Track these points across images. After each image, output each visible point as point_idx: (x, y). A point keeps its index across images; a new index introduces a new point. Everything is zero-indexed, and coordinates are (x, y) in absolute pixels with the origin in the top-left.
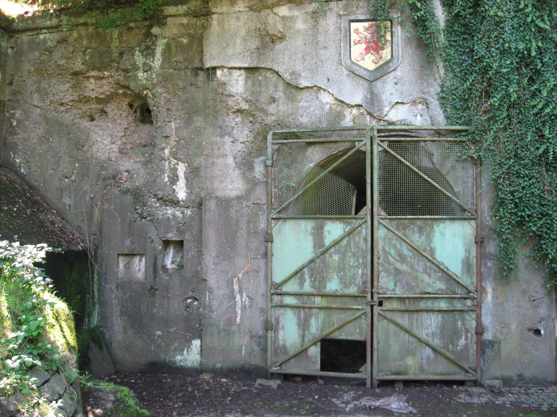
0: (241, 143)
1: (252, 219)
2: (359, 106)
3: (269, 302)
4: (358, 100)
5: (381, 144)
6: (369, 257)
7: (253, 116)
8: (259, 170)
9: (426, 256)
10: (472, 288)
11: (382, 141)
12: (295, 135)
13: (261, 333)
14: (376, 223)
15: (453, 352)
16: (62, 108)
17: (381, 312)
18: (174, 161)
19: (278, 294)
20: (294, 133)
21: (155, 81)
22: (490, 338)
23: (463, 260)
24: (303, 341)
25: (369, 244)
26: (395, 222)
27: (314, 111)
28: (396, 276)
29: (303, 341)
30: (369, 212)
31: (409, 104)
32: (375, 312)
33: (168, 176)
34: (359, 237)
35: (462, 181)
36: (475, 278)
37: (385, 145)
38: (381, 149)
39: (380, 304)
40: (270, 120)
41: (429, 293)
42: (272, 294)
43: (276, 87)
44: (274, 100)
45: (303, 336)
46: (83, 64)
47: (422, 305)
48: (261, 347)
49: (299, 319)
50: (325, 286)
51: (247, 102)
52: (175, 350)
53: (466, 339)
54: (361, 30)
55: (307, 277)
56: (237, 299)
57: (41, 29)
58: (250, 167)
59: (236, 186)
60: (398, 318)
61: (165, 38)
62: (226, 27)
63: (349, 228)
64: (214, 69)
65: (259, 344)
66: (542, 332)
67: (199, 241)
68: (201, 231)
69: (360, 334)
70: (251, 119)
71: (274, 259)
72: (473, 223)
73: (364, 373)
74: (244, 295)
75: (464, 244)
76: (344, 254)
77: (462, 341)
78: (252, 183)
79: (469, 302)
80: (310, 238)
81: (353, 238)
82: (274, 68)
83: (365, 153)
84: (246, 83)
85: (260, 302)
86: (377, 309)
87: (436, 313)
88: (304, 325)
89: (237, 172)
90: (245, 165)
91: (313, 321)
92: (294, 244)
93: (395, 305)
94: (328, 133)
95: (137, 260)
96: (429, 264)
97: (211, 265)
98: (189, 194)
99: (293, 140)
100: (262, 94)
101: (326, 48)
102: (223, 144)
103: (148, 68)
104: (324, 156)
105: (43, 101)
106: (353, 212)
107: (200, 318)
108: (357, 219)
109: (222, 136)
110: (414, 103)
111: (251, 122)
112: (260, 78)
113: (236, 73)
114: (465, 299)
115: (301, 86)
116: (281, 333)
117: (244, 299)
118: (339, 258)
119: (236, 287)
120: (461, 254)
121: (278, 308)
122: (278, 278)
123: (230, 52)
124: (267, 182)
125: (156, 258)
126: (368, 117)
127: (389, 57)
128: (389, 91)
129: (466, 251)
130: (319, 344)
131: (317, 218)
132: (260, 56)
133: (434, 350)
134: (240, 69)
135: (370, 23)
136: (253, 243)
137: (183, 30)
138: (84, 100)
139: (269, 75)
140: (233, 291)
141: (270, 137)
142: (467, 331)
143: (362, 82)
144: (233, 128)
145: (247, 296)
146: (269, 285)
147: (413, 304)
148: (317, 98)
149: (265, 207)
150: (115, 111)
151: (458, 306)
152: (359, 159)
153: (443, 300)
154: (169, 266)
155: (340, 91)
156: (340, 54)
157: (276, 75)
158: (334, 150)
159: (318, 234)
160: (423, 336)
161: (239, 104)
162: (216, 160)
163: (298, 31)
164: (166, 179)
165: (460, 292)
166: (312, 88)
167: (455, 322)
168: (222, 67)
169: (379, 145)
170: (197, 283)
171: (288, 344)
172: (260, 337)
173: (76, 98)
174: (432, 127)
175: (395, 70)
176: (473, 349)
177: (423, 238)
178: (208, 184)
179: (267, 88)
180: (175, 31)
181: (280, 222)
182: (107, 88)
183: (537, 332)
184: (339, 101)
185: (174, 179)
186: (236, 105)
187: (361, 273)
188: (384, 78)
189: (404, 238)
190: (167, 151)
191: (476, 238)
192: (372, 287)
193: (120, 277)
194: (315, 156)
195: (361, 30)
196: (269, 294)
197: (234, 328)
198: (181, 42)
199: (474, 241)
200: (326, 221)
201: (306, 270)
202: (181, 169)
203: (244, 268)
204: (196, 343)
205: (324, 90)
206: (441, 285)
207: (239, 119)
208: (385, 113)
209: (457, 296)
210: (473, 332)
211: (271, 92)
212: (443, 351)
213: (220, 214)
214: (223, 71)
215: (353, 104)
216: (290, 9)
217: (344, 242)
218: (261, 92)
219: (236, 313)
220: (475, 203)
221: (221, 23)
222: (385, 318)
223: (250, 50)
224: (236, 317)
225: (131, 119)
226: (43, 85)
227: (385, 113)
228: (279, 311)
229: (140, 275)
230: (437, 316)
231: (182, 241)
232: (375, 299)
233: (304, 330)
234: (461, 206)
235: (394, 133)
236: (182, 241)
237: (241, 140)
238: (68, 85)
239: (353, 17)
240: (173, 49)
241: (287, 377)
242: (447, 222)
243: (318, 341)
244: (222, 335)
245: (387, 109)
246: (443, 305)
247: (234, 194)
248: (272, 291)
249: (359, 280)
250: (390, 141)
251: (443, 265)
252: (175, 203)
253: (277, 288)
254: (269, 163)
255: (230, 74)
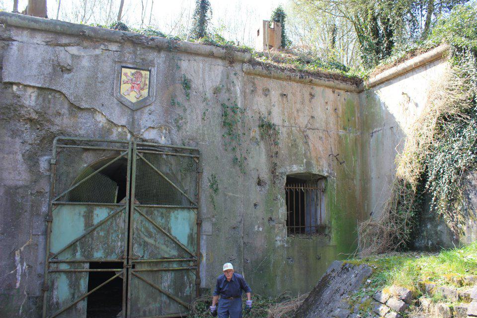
0: (29, 144)
2: (123, 126)
3: (47, 269)
4: (123, 121)
5: (139, 154)
6: (126, 234)
7: (41, 125)
9: (165, 233)
10: (194, 254)
11: (140, 152)
12: (73, 142)
13: (38, 294)
15: (181, 298)
17: (133, 272)
19: (54, 263)
20: (73, 140)
22: (204, 286)
23: (188, 235)
25: (127, 224)
27: (90, 126)
28: (144, 247)
30: (128, 202)
31: (157, 129)
32: (129, 273)
34: (120, 219)
36: (196, 247)
38: (138, 158)
39: (133, 267)
40: (54, 129)
41: (166, 258)
42: (50, 263)
43: (62, 104)
44: (59, 114)
45: (73, 295)
47: (160, 267)
48: (38, 305)
49: (71, 281)
51: (37, 113)
54: (129, 74)
55: (79, 249)
56: (18, 268)
59: (24, 177)
63: (112, 212)
64: (12, 84)
70: (39, 127)
74: (25, 264)
75: (189, 225)
79: (192, 264)
80: (82, 219)
81: (115, 219)
82: (62, 91)
83: (126, 160)
85: (39, 269)
86: (131, 271)
87: (171, 272)
89: (24, 166)
92: (69, 224)
93: (145, 268)
94: (99, 143)
96: (167, 238)
99: (71, 146)
100: (50, 109)
101: (103, 82)
106: (115, 201)
108: (119, 206)
111: (38, 129)
112: (50, 97)
113: (30, 90)
114: (190, 261)
115: (82, 107)
116: (55, 292)
117: (24, 268)
118: (105, 234)
119: (18, 258)
120: (187, 231)
121: (54, 273)
124: (50, 176)
127: (146, 95)
128: (146, 119)
129: (190, 229)
130: (86, 299)
131: (88, 205)
132: (51, 80)
133: (169, 297)
134: (34, 87)
135: (136, 70)
136: (35, 222)
139: (57, 95)
140: (14, 261)
141: (55, 141)
142: (190, 283)
144: (23, 132)
145: (27, 265)
146: (48, 255)
147: (159, 265)
148: (94, 118)
149: (47, 195)
153: (175, 263)
156: (113, 88)
157: (63, 96)
158: (103, 156)
159: (88, 217)
161: (30, 114)
162: (6, 156)
163: (83, 67)
165: (187, 257)
166: (90, 109)
167: (183, 277)
168: (18, 84)
169: (137, 155)
171: (60, 301)
172: (37, 298)
174: (173, 146)
175: (150, 105)
177: (163, 221)
179: (55, 105)
181: (59, 207)
184: (109, 121)
186: (27, 115)
188: (142, 109)
189: (151, 220)
191: (197, 220)
192: (128, 255)
194: (89, 159)
195: (129, 74)
196: (47, 263)
199: (196, 223)
200: (95, 207)
201: (78, 243)
203: (25, 243)
205: (99, 112)
206: (174, 253)
207: (28, 126)
208: (141, 133)
209: (185, 259)
210: (194, 283)
214: (18, 86)
215: (120, 124)
216: (79, 50)
217: (109, 223)
218: (49, 108)
219: (17, 279)
223: (44, 74)
224: (16, 283)
227: (141, 133)
228: (54, 276)
230: (172, 274)
234: (189, 200)
235: (146, 148)
237: (30, 142)
243: (86, 297)
245: (143, 130)
246: (175, 266)
248: (50, 260)
249: (118, 251)
250: (144, 153)
251: (176, 238)
253: (54, 258)
254: (53, 161)
255: (25, 91)
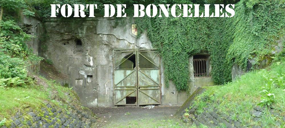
1: (109, 70)
8: (111, 58)
9: (149, 77)
10: (159, 84)
12: (119, 50)
14: (138, 70)
15: (155, 98)
16: (58, 42)
18: (89, 56)
21: (84, 36)
24: (122, 97)
26: (142, 70)
29: (122, 97)
33: (88, 60)
35: (157, 61)
37: (140, 53)
39: (139, 88)
46: (64, 31)
49: (121, 93)
50: (127, 85)
52: (91, 102)
53: (158, 95)
55: (123, 83)
57: (52, 21)
58: (108, 58)
60: (143, 91)
61: (86, 26)
62: (102, 24)
65: (112, 99)
66: (174, 93)
67: (97, 75)
68: (97, 73)
69: (135, 95)
71: (115, 79)
72: (159, 70)
73: (136, 104)
76: (131, 78)
77: (157, 96)
78: (109, 62)
80: (123, 74)
84: (107, 38)
85: (112, 89)
86: (138, 89)
88: (122, 94)
89: (105, 59)
90: (107, 56)
91: (124, 93)
92: (119, 75)
93: (143, 88)
95: (80, 80)
96: (150, 79)
97: (100, 81)
98: (94, 64)
99: (119, 52)
102: (102, 52)
103: (82, 33)
104: (126, 55)
105: (53, 40)
107: (97, 94)
109: (101, 51)
110: (146, 43)
113: (105, 35)
116: (117, 96)
119: (106, 86)
120: (156, 77)
122: (116, 83)
123: (103, 30)
125: (85, 80)
126: (136, 46)
130: (126, 98)
137: (91, 24)
138: (63, 40)
140: (105, 87)
142: (158, 93)
143: (134, 38)
147: (147, 88)
149: (112, 67)
150: (71, 42)
151: (156, 88)
152: (134, 56)
154: (89, 81)
155: (129, 40)
159: (125, 73)
160: (149, 95)
164: (87, 61)
167: (156, 92)
168: (101, 34)
170: (96, 85)
173: (61, 39)
176: (160, 98)
177: (148, 73)
178: (98, 62)
180: (89, 24)
182: (70, 37)
183: (173, 93)
185: (89, 61)
187: (135, 82)
190: (87, 54)
193: (76, 85)
194: (124, 55)
197: (105, 95)
198: (91, 27)
202: (91, 58)
204: (96, 99)
211: (113, 40)
212: (153, 98)
213: (101, 69)
220: (67, 41)
221: (101, 23)
222: (140, 91)
225: (75, 44)
226: (52, 36)
229: (81, 84)
231: (92, 76)
232: (138, 87)
233: (122, 95)
236: (92, 76)
238: (59, 36)
239: (132, 23)
240: (88, 29)
241: (118, 106)
242: (154, 70)
244: (103, 97)
246: (153, 88)
247: (105, 64)
249: (134, 83)
252: (90, 66)
254: (113, 57)
255: (103, 36)
